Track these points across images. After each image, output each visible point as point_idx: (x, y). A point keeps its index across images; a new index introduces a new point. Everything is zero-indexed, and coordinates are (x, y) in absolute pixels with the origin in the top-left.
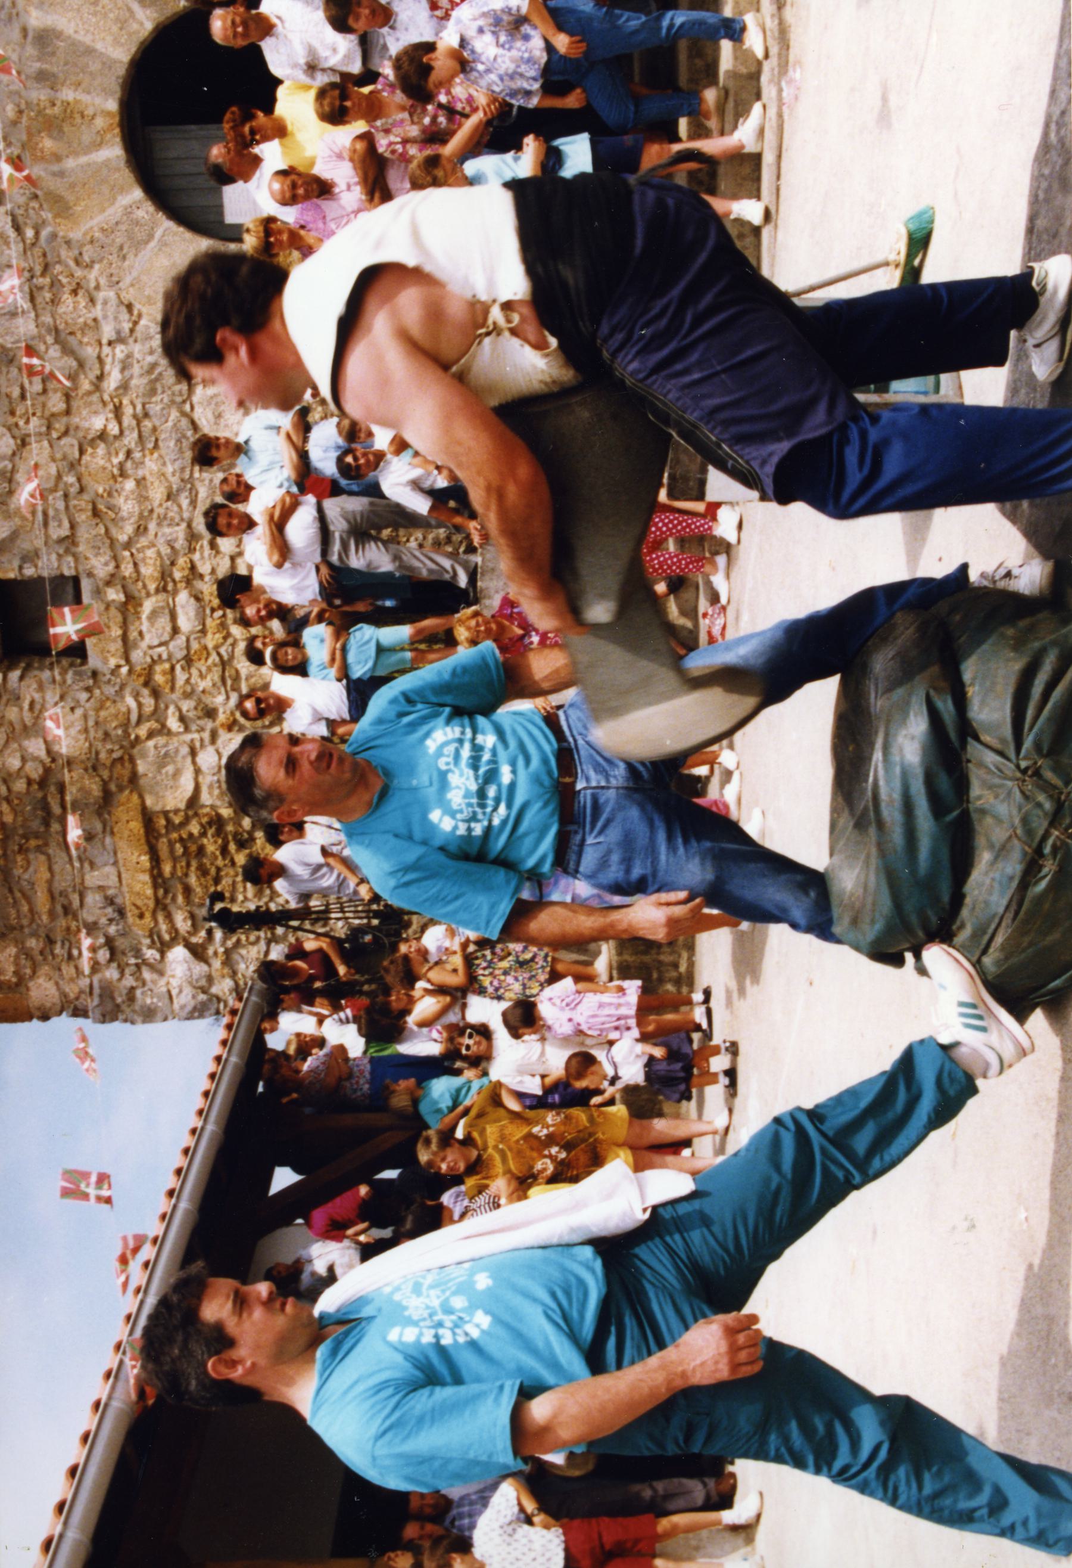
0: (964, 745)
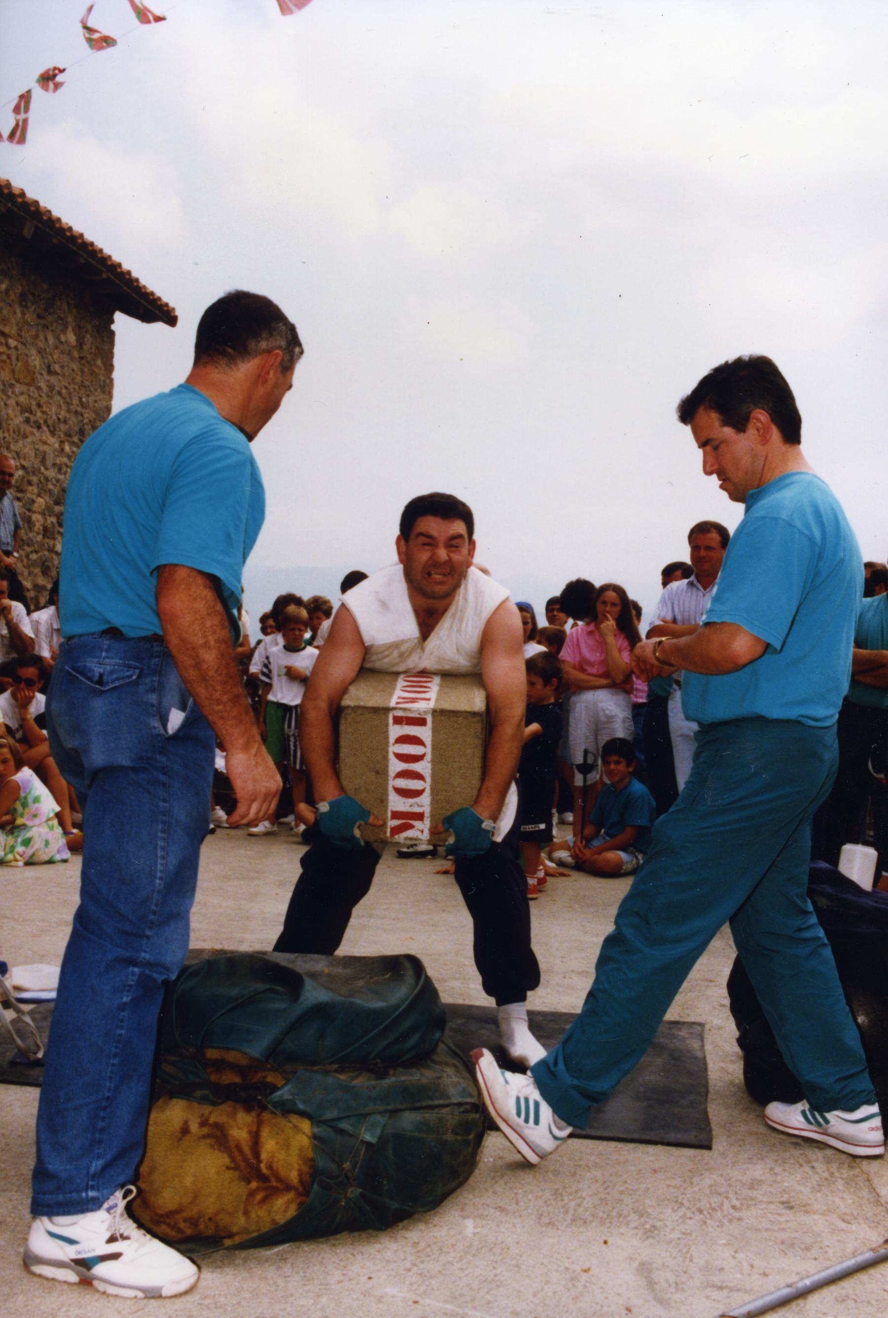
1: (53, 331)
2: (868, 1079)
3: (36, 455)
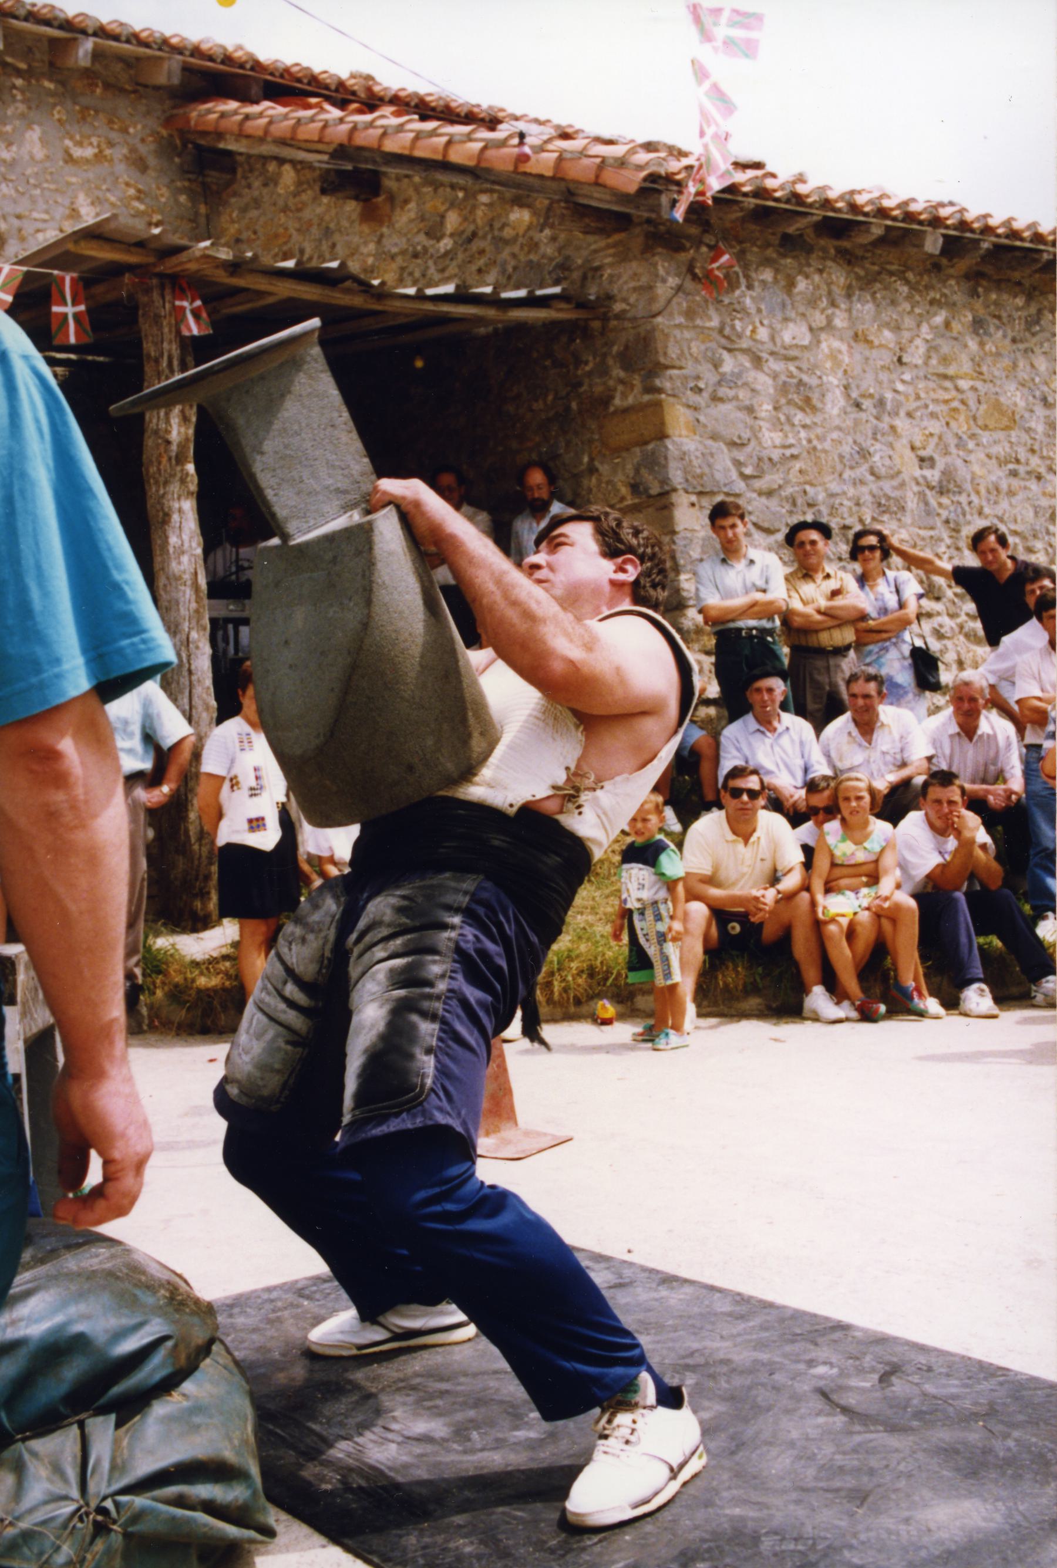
1: (1045, 353)
2: (486, 772)
3: (1036, 513)
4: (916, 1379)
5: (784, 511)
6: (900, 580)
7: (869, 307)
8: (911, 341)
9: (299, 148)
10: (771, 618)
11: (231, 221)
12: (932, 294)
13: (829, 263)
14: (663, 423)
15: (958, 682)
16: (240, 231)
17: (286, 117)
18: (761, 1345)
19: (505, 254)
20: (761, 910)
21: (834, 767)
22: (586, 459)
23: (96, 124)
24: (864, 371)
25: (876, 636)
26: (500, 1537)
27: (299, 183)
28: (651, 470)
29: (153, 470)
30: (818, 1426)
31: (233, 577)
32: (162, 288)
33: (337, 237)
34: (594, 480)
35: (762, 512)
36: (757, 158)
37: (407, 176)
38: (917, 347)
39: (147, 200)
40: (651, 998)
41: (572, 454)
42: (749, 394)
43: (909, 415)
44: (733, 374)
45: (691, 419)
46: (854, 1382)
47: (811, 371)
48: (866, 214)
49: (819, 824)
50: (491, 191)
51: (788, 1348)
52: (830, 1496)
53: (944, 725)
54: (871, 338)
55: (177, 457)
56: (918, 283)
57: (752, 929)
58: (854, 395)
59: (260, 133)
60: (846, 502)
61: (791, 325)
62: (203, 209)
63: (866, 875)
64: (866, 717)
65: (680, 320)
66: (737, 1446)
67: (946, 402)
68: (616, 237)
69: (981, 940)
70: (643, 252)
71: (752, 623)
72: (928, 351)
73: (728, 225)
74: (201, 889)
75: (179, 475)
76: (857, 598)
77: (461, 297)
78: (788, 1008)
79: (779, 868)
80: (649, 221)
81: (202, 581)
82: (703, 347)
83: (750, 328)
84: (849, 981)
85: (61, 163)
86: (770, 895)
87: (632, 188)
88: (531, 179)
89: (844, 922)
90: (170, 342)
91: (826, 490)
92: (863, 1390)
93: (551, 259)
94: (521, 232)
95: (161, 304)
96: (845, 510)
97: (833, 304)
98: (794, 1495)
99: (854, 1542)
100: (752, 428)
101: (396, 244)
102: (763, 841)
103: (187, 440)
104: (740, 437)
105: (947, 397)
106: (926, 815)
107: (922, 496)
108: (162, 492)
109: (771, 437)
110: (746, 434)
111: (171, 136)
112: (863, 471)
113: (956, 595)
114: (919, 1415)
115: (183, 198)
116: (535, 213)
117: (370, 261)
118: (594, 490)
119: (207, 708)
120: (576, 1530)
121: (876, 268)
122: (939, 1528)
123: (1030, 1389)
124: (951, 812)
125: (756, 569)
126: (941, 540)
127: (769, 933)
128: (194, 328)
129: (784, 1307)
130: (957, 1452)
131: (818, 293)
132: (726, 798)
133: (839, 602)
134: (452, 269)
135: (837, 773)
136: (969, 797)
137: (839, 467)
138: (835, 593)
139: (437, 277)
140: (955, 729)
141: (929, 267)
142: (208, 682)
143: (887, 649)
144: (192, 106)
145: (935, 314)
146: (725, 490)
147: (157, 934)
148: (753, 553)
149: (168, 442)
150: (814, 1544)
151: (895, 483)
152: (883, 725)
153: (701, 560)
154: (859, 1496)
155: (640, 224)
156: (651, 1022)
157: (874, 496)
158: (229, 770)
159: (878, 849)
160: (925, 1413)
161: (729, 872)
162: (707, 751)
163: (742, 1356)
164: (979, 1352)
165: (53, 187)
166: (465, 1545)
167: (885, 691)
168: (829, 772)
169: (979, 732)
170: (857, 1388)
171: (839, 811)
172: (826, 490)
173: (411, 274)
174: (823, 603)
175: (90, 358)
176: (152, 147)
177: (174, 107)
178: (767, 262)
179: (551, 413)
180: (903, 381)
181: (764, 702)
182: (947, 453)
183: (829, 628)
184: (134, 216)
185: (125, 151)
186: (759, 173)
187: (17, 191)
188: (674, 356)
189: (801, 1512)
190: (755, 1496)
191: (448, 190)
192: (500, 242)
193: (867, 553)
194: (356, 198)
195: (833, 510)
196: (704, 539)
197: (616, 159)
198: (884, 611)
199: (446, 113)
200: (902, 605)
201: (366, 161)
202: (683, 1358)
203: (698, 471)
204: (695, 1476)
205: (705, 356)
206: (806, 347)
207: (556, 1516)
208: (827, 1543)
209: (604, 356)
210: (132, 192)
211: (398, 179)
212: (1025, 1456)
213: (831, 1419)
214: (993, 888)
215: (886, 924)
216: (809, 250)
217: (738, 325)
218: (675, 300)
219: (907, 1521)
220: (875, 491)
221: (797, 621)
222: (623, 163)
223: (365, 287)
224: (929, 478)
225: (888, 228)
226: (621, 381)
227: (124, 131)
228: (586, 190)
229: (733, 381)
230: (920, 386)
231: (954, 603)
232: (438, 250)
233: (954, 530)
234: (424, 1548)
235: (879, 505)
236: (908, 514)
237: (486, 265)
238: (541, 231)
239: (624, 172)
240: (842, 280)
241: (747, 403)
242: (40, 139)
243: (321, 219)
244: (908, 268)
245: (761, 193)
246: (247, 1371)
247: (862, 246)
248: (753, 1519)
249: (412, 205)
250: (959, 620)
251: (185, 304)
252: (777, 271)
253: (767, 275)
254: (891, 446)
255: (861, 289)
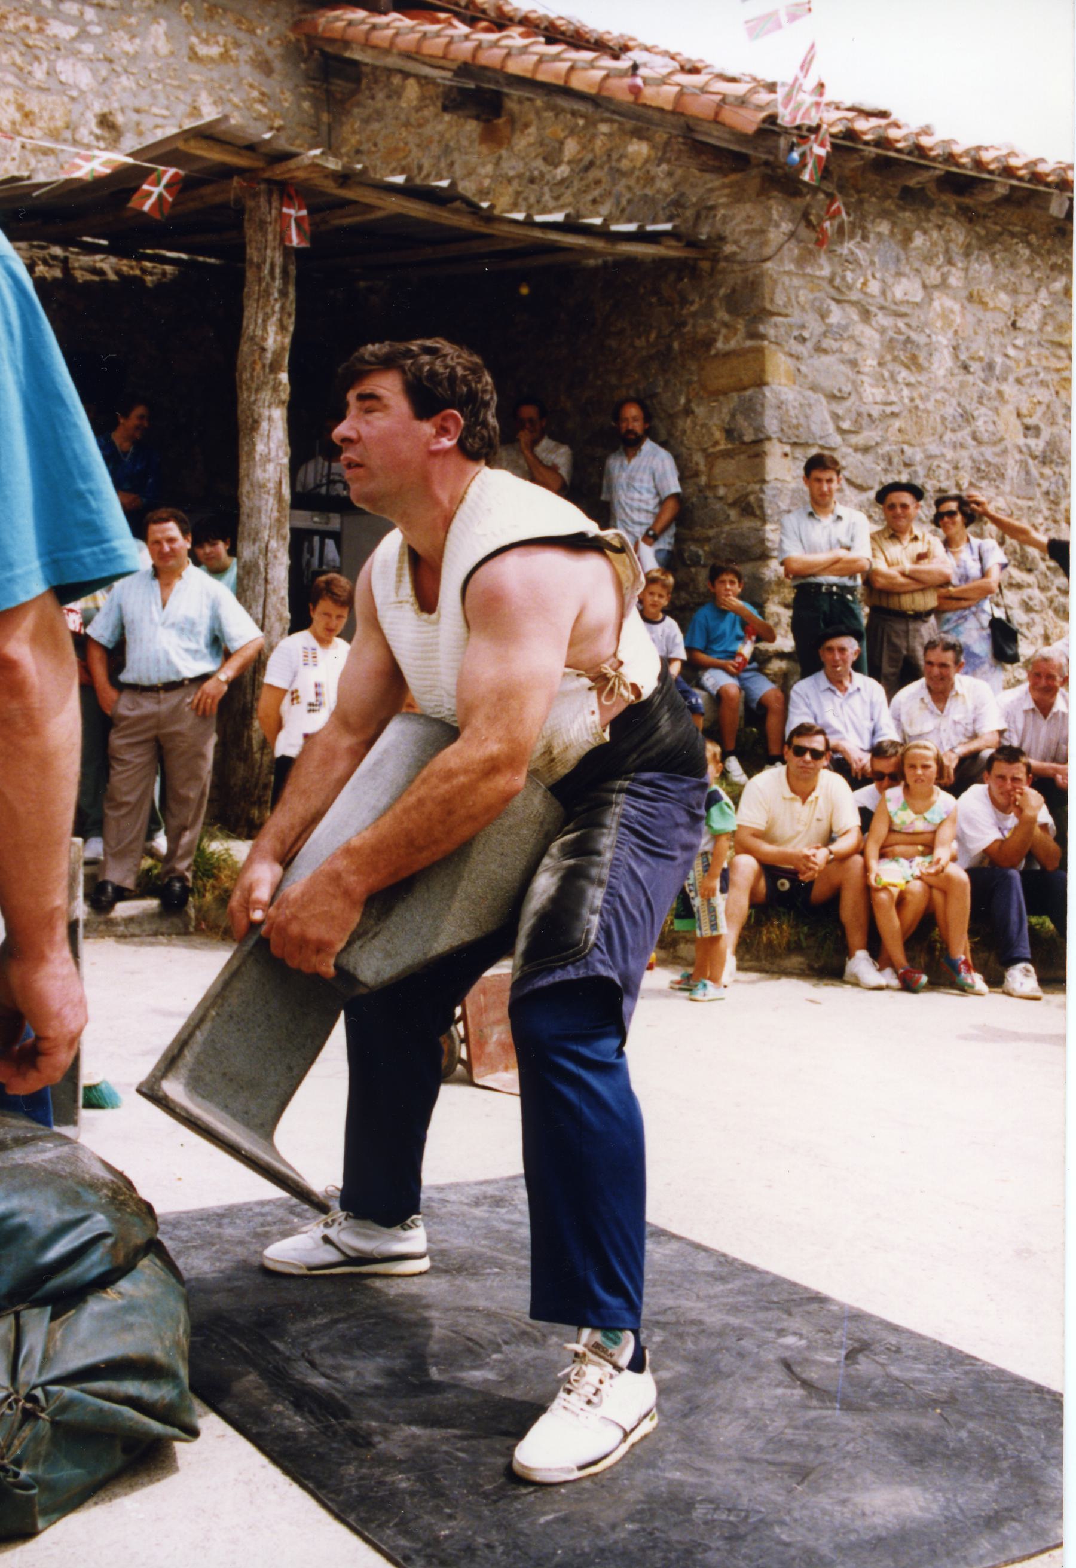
0: (40, 1303)
4: (882, 1359)
5: (879, 468)
6: (984, 548)
7: (988, 267)
8: (1027, 306)
9: (424, 63)
10: (852, 576)
11: (352, 132)
12: (1054, 259)
13: (949, 220)
14: (763, 371)
15: (1037, 657)
16: (360, 143)
17: (412, 30)
18: (734, 1309)
19: (620, 187)
20: (811, 869)
21: (903, 733)
22: (683, 400)
23: (224, 23)
24: (976, 333)
25: (954, 604)
26: (439, 1476)
27: (422, 98)
28: (747, 417)
29: (246, 376)
30: (776, 1397)
31: (323, 490)
32: (270, 193)
33: (456, 156)
34: (689, 421)
35: (857, 467)
36: (882, 107)
37: (529, 99)
38: (1033, 313)
39: (270, 104)
40: (693, 947)
41: (669, 394)
42: (854, 348)
43: (1019, 381)
44: (839, 325)
45: (792, 368)
46: (819, 1356)
47: (920, 329)
48: (991, 172)
49: (881, 790)
50: (611, 121)
51: (761, 1315)
52: (772, 1468)
53: (1019, 699)
54: (986, 299)
55: (271, 365)
56: (1040, 246)
57: (801, 889)
58: (963, 357)
59: (386, 45)
60: (944, 465)
61: (904, 280)
62: (325, 117)
63: (922, 845)
64: (941, 687)
65: (791, 267)
66: (691, 1409)
67: (1058, 371)
68: (734, 177)
69: (1034, 920)
70: (758, 195)
71: (833, 579)
72: (1044, 317)
73: (847, 172)
74: (259, 798)
75: (271, 383)
76: (943, 563)
77: (569, 226)
78: (830, 969)
79: (835, 829)
80: (767, 163)
81: (286, 491)
82: (811, 297)
83: (861, 280)
84: (895, 947)
85: (186, 60)
86: (821, 856)
87: (751, 129)
88: (650, 112)
89: (895, 891)
90: (274, 249)
91: (925, 451)
92: (828, 1366)
93: (666, 195)
94: (638, 164)
95: (266, 209)
96: (942, 472)
97: (950, 262)
98: (737, 1465)
99: (787, 1518)
100: (854, 382)
101: (513, 168)
102: (820, 801)
103: (283, 348)
104: (840, 390)
105: (1060, 365)
106: (989, 789)
107: (1024, 465)
108: (253, 398)
109: (872, 393)
110: (847, 388)
111: (298, 40)
112: (964, 434)
113: (1049, 568)
114: (877, 1396)
115: (306, 105)
116: (653, 147)
117: (487, 182)
118: (689, 432)
119: (281, 618)
120: (517, 1479)
121: (998, 228)
122: (874, 1513)
123: (994, 1381)
124: (1014, 789)
125: (842, 526)
126: (1040, 511)
127: (819, 892)
128: (295, 241)
129: (767, 1273)
130: (907, 1437)
131: (935, 250)
132: (789, 754)
133: (924, 566)
134: (568, 198)
135: (906, 738)
136: (1034, 775)
137: (940, 429)
138: (921, 557)
139: (551, 204)
140: (1030, 704)
141: (1053, 230)
142: (284, 592)
143: (965, 618)
144: (322, 12)
145: (1055, 280)
146: (821, 442)
147: (213, 838)
148: (840, 509)
149: (263, 350)
150: (747, 1517)
151: (997, 449)
152: (957, 694)
153: (789, 511)
154: (802, 1473)
155: (758, 166)
156: (691, 970)
157: (974, 461)
158: (292, 682)
159: (938, 820)
160: (884, 1394)
161: (784, 828)
162: (776, 706)
163: (714, 1319)
164: (950, 1339)
165: (175, 83)
166: (401, 1480)
167: (962, 659)
168: (896, 737)
169: (1054, 710)
170: (822, 1363)
171: (904, 777)
172: (925, 451)
173: (526, 199)
174: (908, 566)
175: (201, 259)
176: (280, 51)
177: (305, 12)
178: (885, 214)
179: (653, 351)
180: (1015, 346)
181: (835, 661)
182: (1053, 423)
183: (913, 592)
184: (256, 119)
185: (251, 52)
186: (883, 122)
187: (138, 84)
188: (781, 303)
189: (740, 1483)
190: (699, 1462)
191: (569, 116)
192: (617, 173)
193: (946, 519)
194: (477, 118)
195: (930, 472)
196: (794, 491)
197: (737, 98)
198: (966, 578)
199: (577, 40)
200: (984, 574)
201: (489, 81)
202: (658, 1313)
203: (794, 421)
204: (646, 1436)
205: (812, 305)
206: (917, 304)
207: (501, 1461)
208: (760, 1516)
209: (711, 297)
210: (255, 94)
211: (520, 101)
212: (975, 1449)
213: (788, 1391)
214: (1050, 868)
215: (938, 896)
216: (929, 204)
217: (849, 276)
218: (786, 247)
219: (844, 1502)
220: (975, 455)
221: (881, 582)
222: (743, 102)
223: (473, 208)
224: (1033, 446)
225: (1013, 188)
226: (726, 325)
227: (252, 32)
228: (705, 127)
229: (840, 333)
230: (1033, 352)
231: (1046, 576)
232: (554, 177)
233: (1053, 502)
234: (361, 1478)
235: (979, 470)
236: (1007, 482)
237: (601, 196)
238: (658, 165)
239: (743, 112)
240: (961, 239)
241: (851, 356)
242: (166, 34)
243: (442, 136)
244: (1031, 230)
245: (883, 142)
246: (192, 1292)
247: (984, 205)
248: (692, 1485)
249: (532, 130)
250: (1049, 594)
251: (292, 212)
252: (894, 224)
253: (884, 227)
254: (996, 410)
255: (980, 249)
